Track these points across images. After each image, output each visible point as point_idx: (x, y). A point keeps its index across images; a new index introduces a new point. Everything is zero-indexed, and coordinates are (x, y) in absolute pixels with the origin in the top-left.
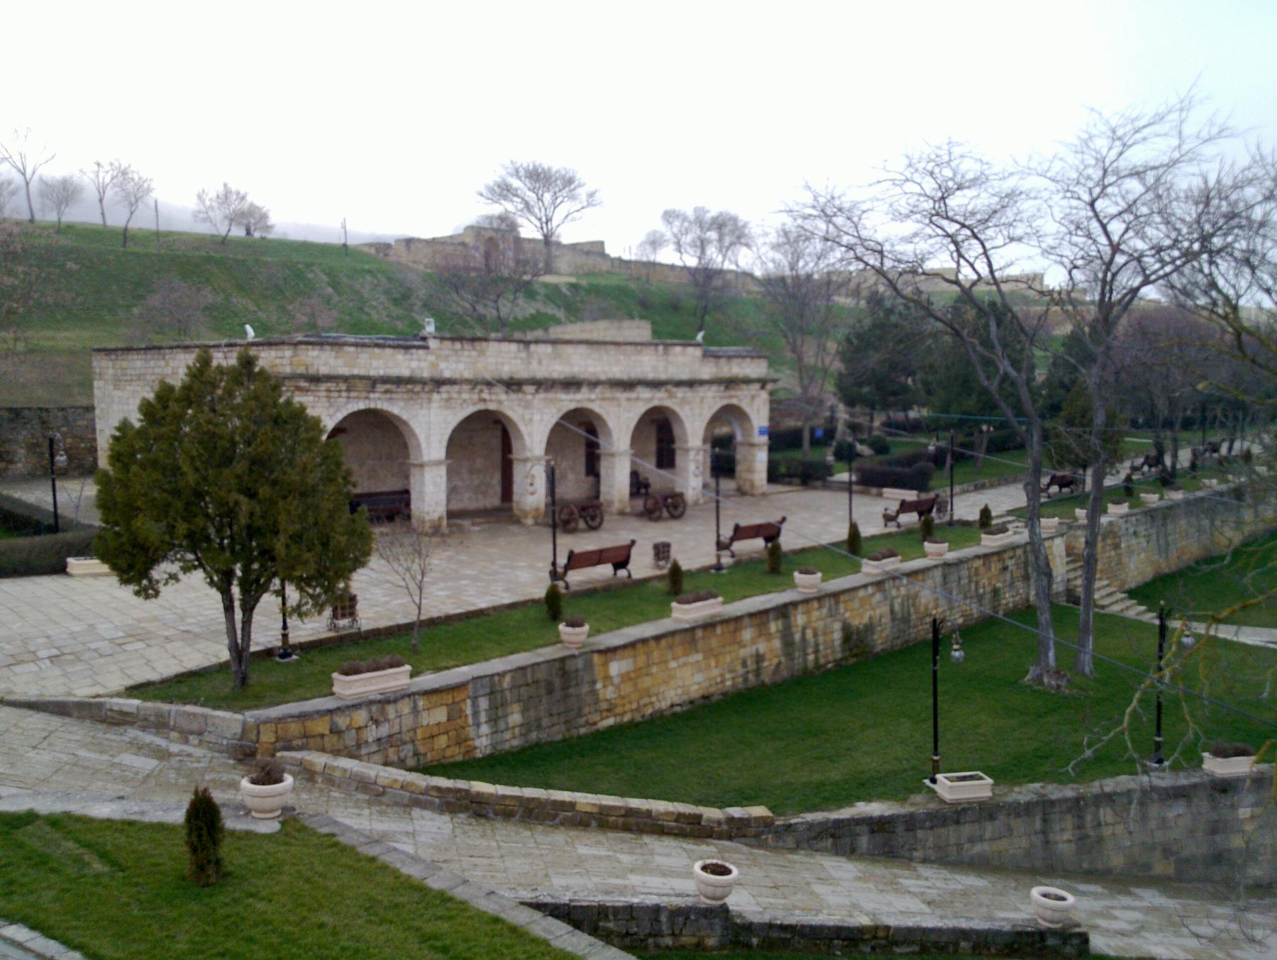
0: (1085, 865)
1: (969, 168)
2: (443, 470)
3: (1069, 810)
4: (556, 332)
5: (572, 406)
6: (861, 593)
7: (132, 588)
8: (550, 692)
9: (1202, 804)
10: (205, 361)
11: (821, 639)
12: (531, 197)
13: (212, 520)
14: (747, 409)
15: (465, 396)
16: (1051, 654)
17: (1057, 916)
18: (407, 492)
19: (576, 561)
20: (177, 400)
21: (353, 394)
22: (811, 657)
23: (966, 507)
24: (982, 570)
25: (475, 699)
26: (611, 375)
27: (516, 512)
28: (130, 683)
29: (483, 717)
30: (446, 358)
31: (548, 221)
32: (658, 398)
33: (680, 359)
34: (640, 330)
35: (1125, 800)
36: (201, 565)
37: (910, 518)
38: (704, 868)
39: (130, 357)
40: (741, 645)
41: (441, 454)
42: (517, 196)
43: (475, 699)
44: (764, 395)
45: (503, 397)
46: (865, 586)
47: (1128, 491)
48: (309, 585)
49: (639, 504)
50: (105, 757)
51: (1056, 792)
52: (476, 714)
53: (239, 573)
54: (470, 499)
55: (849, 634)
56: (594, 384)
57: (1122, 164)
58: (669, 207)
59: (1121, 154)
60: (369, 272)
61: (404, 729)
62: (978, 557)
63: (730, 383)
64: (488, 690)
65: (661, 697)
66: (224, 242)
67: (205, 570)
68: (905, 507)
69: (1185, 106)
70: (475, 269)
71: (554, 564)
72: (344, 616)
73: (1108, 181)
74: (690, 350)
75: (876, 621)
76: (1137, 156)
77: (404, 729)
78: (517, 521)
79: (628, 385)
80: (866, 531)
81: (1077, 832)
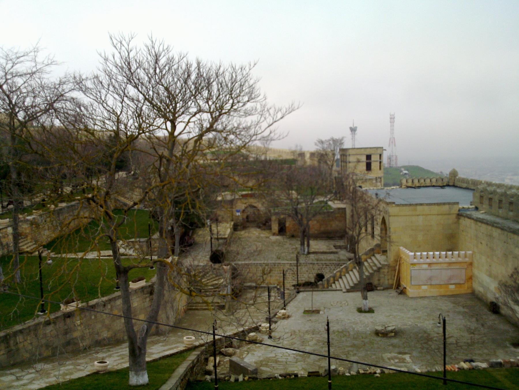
0: (12, 362)
17: (190, 343)
35: (28, 331)
38: (98, 363)
47: (42, 205)
57: (13, 70)
59: (12, 67)
76: (20, 68)
81: (7, 349)
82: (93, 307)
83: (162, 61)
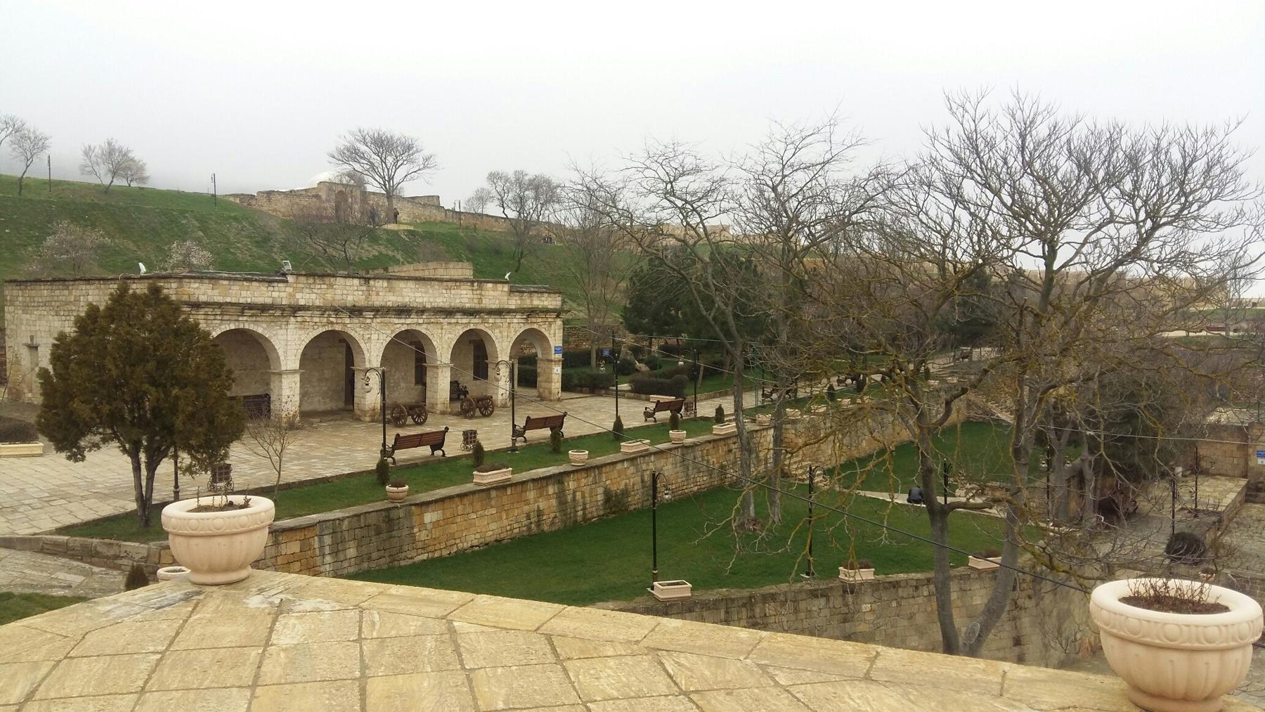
1: (689, 163)
2: (297, 378)
3: (744, 605)
4: (394, 270)
5: (404, 328)
6: (619, 466)
7: (64, 455)
8: (378, 533)
9: (837, 602)
10: (124, 290)
11: (588, 499)
12: (376, 159)
13: (127, 403)
14: (546, 334)
15: (316, 320)
16: (752, 508)
18: (267, 396)
19: (401, 443)
20: (103, 317)
21: (226, 317)
22: (580, 513)
23: (706, 409)
24: (712, 451)
25: (320, 536)
26: (435, 305)
27: (358, 412)
28: (59, 525)
29: (327, 550)
30: (301, 290)
31: (391, 178)
32: (474, 323)
33: (492, 293)
34: (464, 270)
36: (117, 438)
37: (665, 415)
39: (38, 287)
40: (527, 502)
41: (297, 366)
42: (364, 158)
43: (320, 536)
44: (559, 322)
45: (347, 321)
46: (622, 461)
48: (197, 452)
49: (457, 406)
50: (45, 574)
51: (735, 593)
52: (322, 547)
53: (145, 443)
54: (319, 401)
55: (608, 495)
56: (421, 311)
58: (493, 170)
60: (235, 219)
61: (268, 557)
62: (709, 442)
63: (531, 312)
64: (331, 531)
65: (463, 539)
66: (106, 191)
67: (119, 440)
68: (660, 407)
69: (832, 124)
70: (326, 217)
71: (384, 445)
72: (221, 480)
73: (786, 172)
74: (500, 287)
75: (630, 487)
76: (806, 156)
77: (268, 557)
78: (358, 420)
79: (449, 312)
80: (627, 424)
82: (895, 585)
83: (1041, 131)
